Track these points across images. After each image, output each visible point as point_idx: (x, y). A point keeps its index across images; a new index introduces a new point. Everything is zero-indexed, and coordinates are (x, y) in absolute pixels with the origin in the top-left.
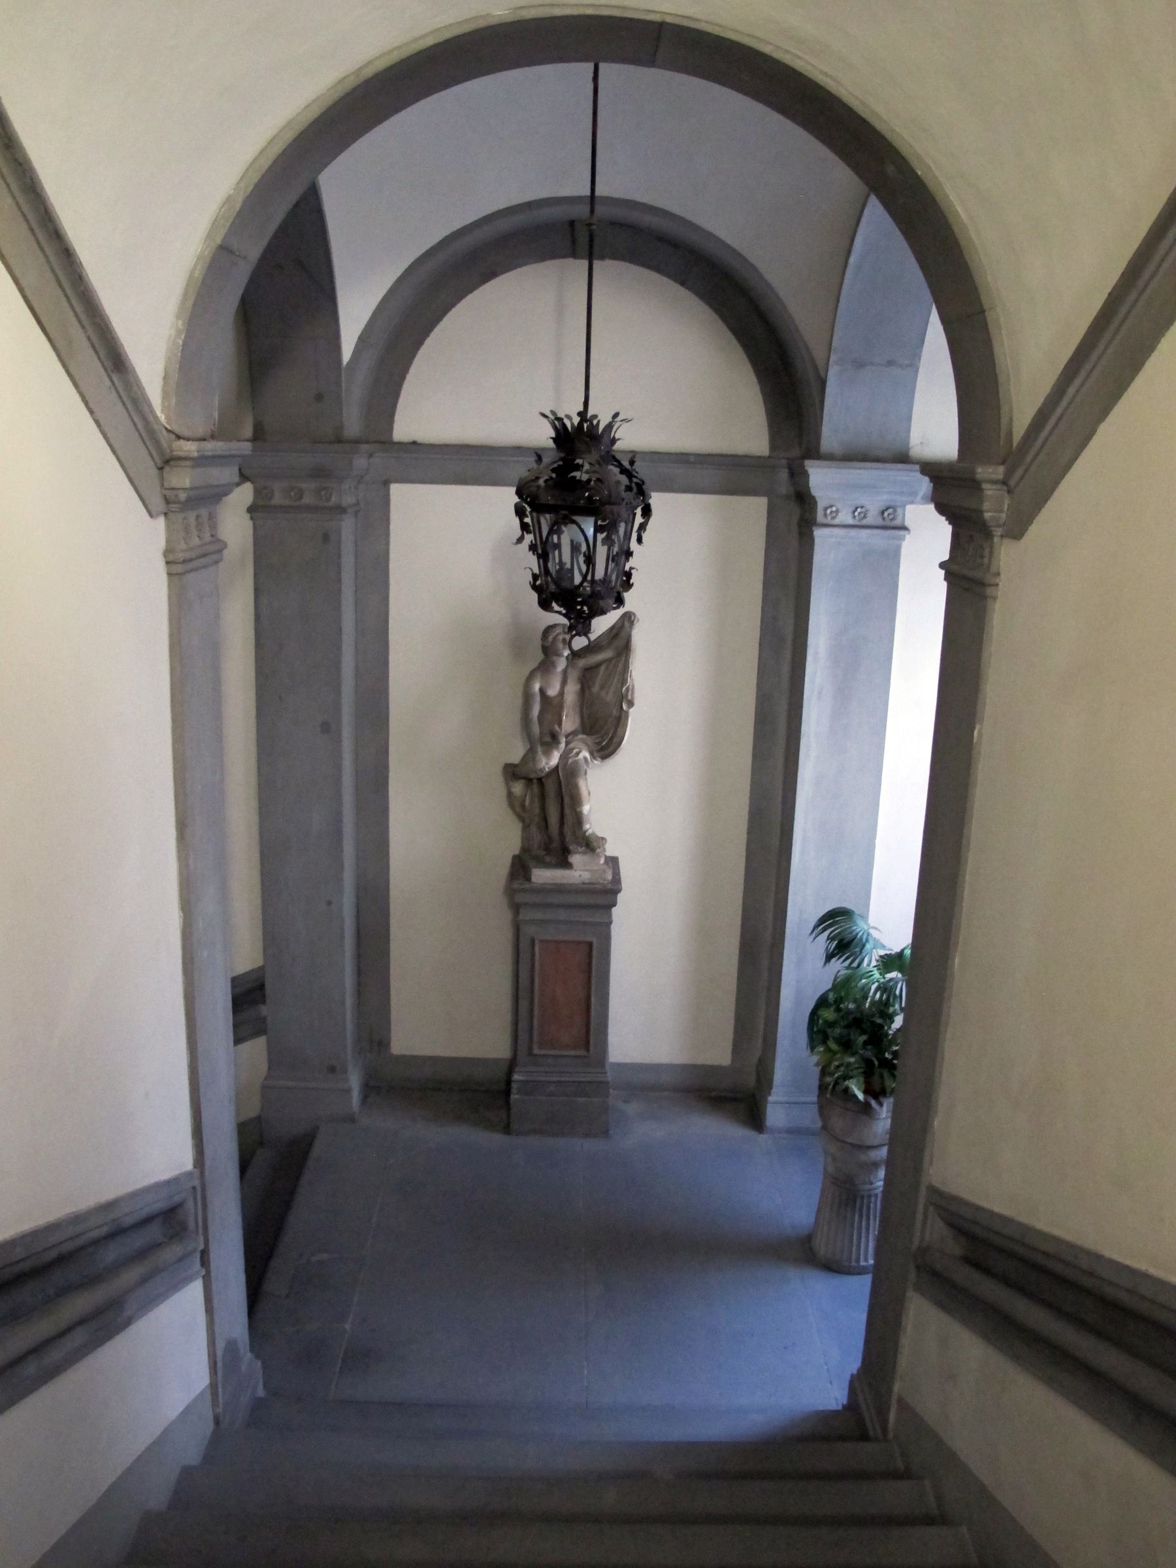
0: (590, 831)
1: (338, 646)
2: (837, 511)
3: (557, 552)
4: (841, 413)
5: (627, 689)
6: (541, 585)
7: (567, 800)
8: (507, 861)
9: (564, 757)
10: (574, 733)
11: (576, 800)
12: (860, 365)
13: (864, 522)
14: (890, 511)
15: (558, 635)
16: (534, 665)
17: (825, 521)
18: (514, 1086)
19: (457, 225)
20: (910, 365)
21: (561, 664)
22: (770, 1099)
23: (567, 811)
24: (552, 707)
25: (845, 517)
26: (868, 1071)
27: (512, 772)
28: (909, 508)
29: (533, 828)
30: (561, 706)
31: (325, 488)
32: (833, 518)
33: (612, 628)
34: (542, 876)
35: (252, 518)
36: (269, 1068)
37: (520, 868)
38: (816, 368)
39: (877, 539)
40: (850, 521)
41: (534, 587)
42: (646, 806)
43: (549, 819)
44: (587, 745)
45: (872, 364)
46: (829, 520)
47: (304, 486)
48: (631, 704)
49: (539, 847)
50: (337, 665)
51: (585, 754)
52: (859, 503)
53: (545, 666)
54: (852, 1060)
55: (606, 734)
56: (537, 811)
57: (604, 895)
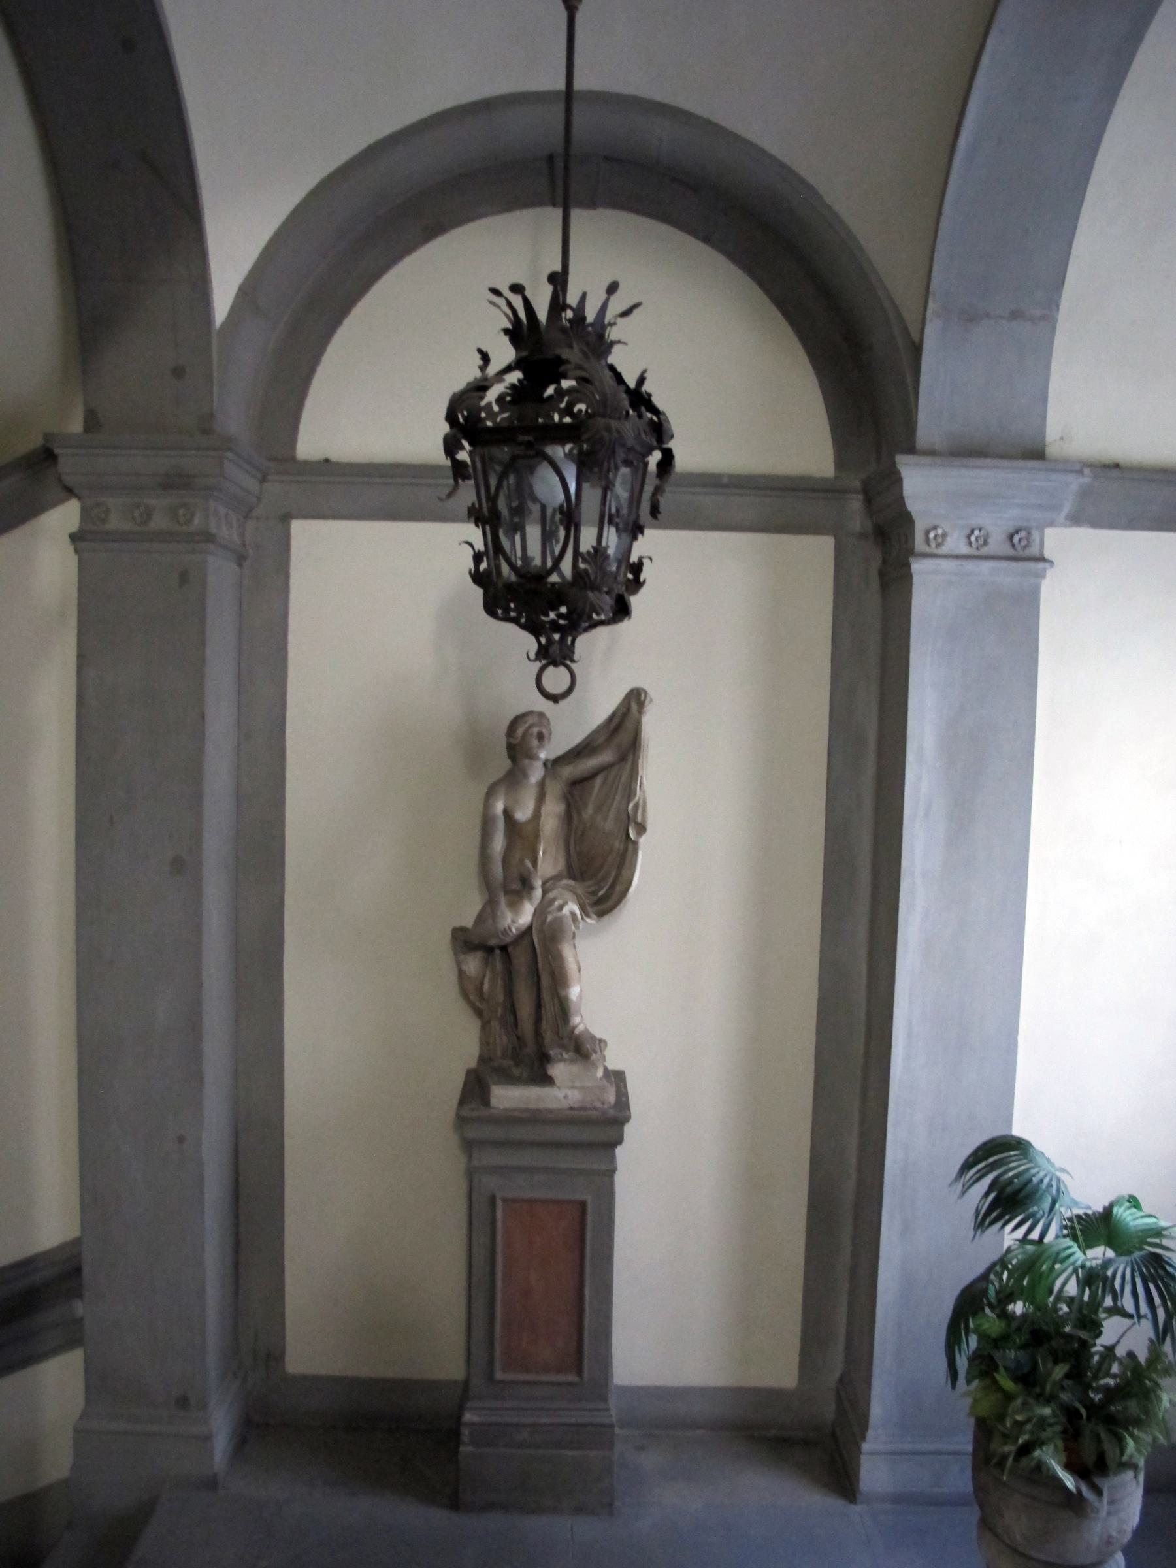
0: (581, 1027)
1: (199, 737)
2: (944, 535)
3: (518, 538)
4: (948, 385)
5: (636, 806)
6: (488, 572)
7: (545, 981)
8: (457, 1081)
9: (540, 912)
10: (557, 878)
11: (559, 980)
12: (971, 317)
13: (985, 551)
14: (1023, 534)
15: (531, 726)
16: (500, 774)
17: (927, 550)
18: (465, 1432)
19: (387, 131)
20: (1044, 318)
21: (536, 773)
22: (866, 1447)
23: (546, 996)
24: (521, 836)
25: (955, 543)
26: (1072, 1435)
27: (465, 941)
28: (1048, 531)
29: (495, 1025)
30: (537, 836)
31: (184, 505)
32: (938, 545)
33: (611, 718)
34: (507, 1097)
35: (76, 551)
36: (88, 1401)
37: (475, 1088)
38: (906, 330)
39: (1006, 575)
40: (964, 550)
41: (478, 578)
42: (665, 991)
43: (518, 1003)
44: (575, 893)
45: (988, 315)
46: (933, 549)
47: (153, 502)
48: (642, 829)
49: (504, 1056)
50: (195, 771)
51: (573, 907)
52: (976, 522)
53: (513, 778)
54: (1047, 1411)
55: (604, 879)
56: (501, 997)
57: (603, 1127)
